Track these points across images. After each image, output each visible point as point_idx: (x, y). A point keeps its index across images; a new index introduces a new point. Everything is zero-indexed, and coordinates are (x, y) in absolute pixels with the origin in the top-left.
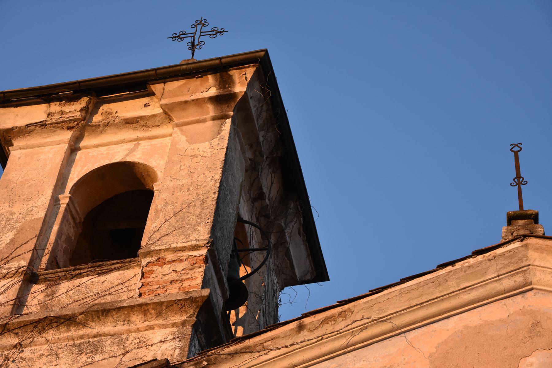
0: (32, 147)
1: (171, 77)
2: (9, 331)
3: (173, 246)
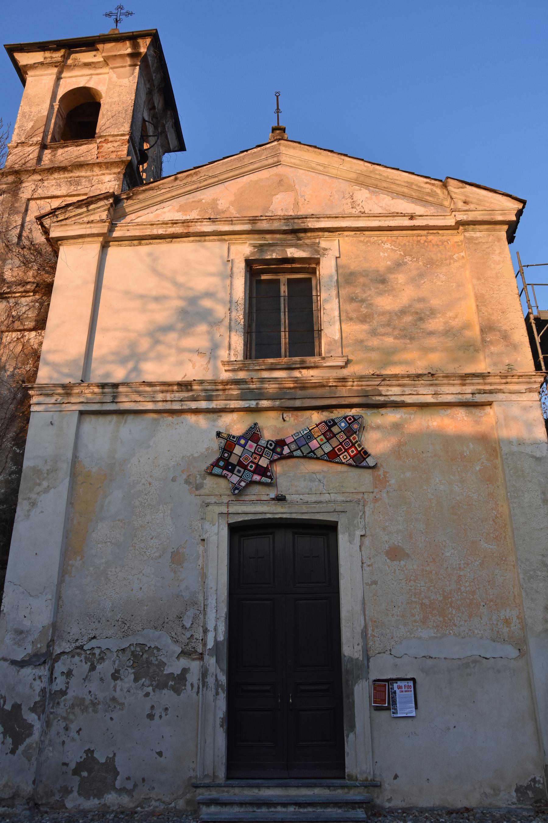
0: (38, 76)
1: (107, 41)
2: (36, 172)
3: (112, 133)
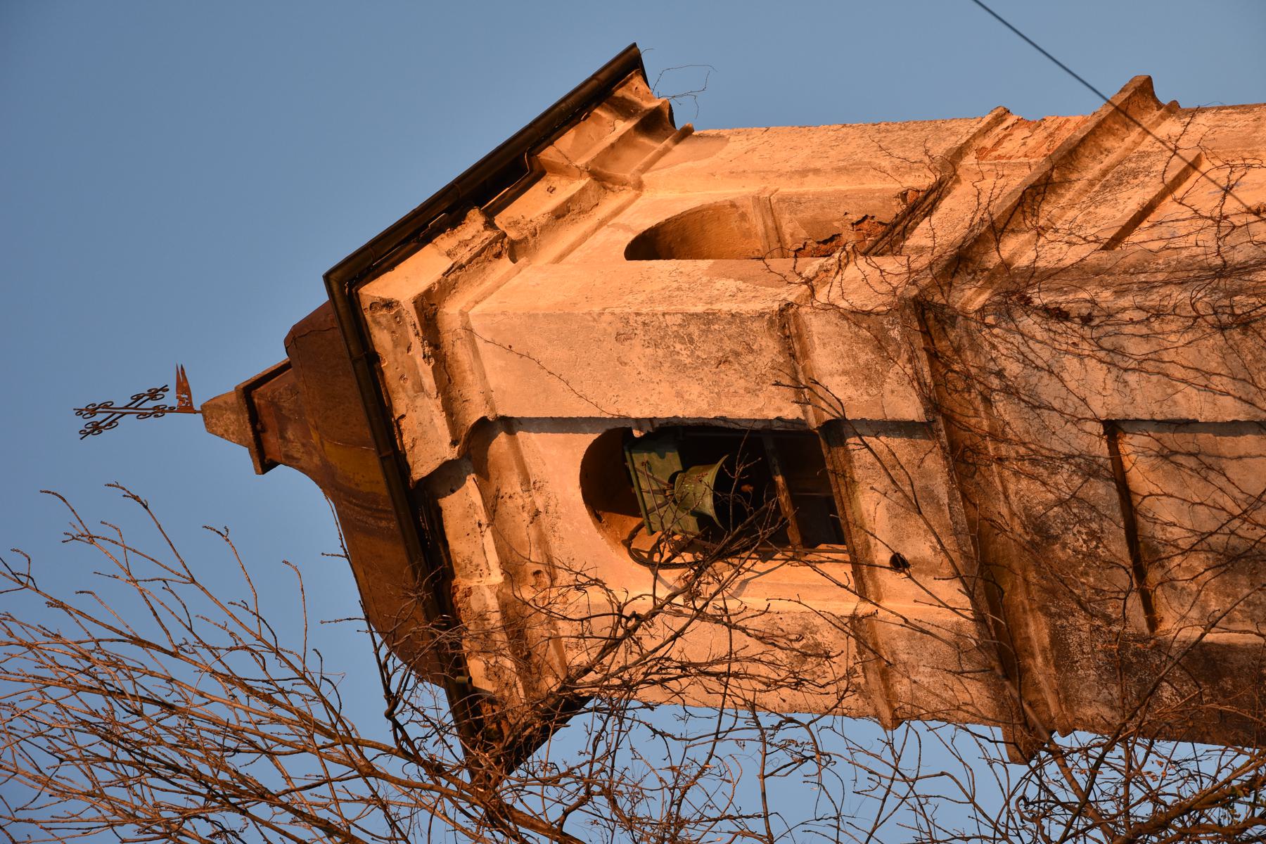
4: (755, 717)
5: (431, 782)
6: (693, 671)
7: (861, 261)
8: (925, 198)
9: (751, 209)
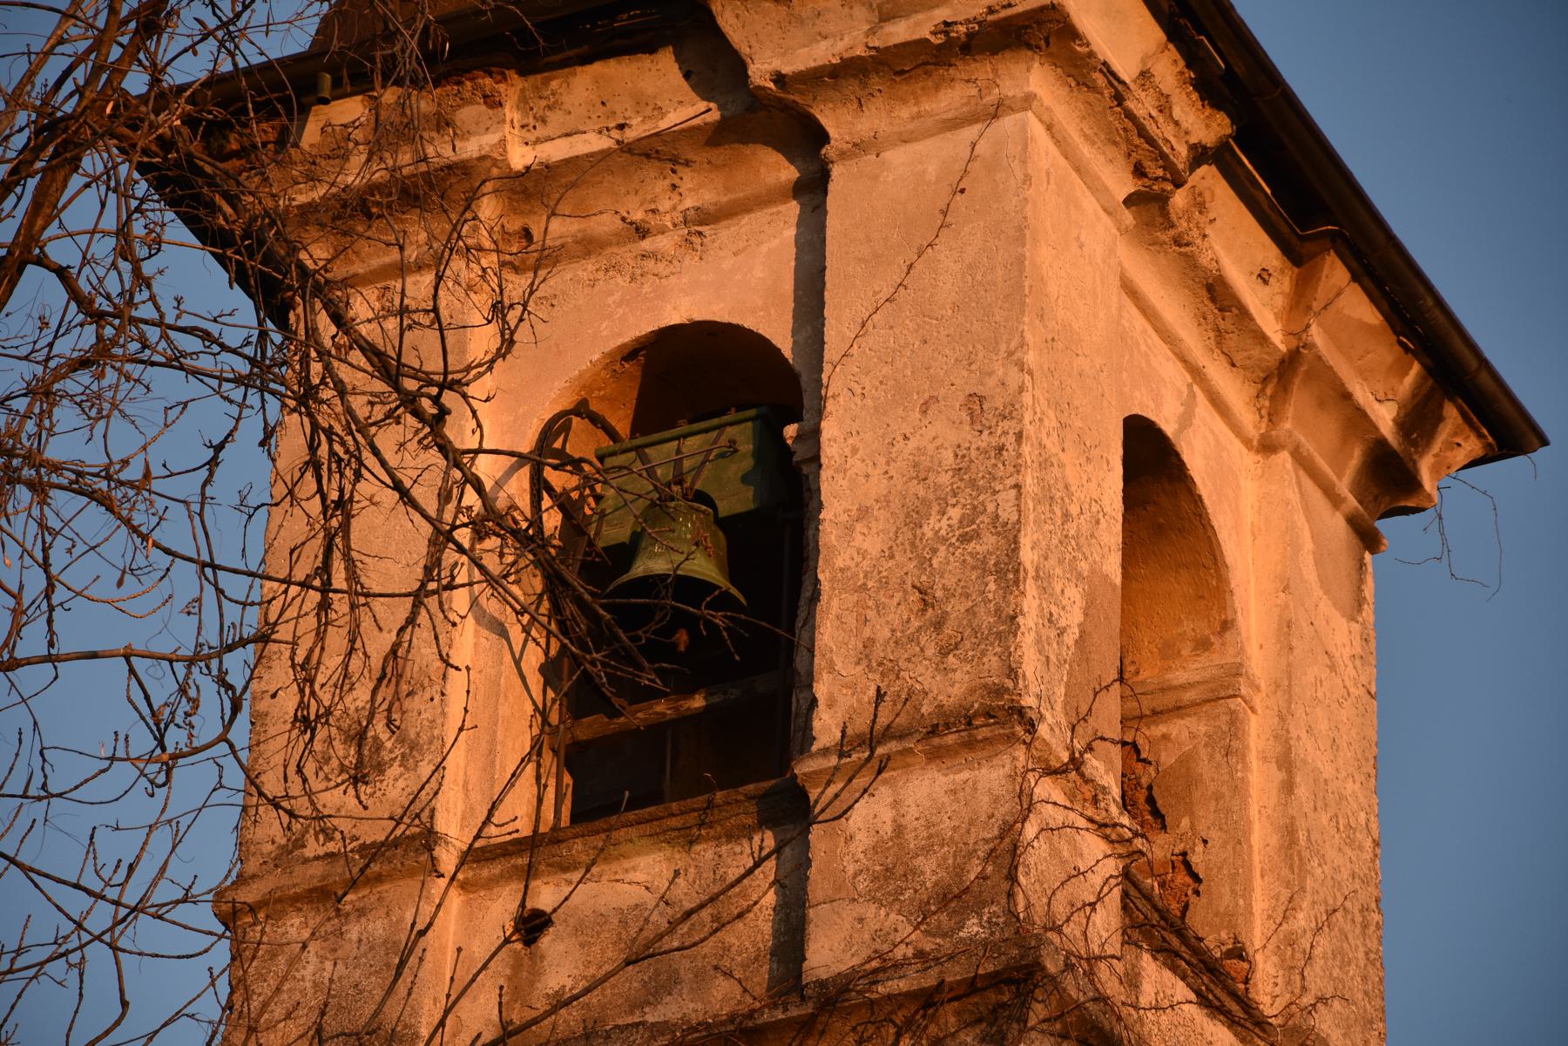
1: (1380, 284)
4: (243, 643)
5: (124, 11)
6: (334, 523)
7: (1112, 867)
8: (1234, 995)
9: (1217, 659)
